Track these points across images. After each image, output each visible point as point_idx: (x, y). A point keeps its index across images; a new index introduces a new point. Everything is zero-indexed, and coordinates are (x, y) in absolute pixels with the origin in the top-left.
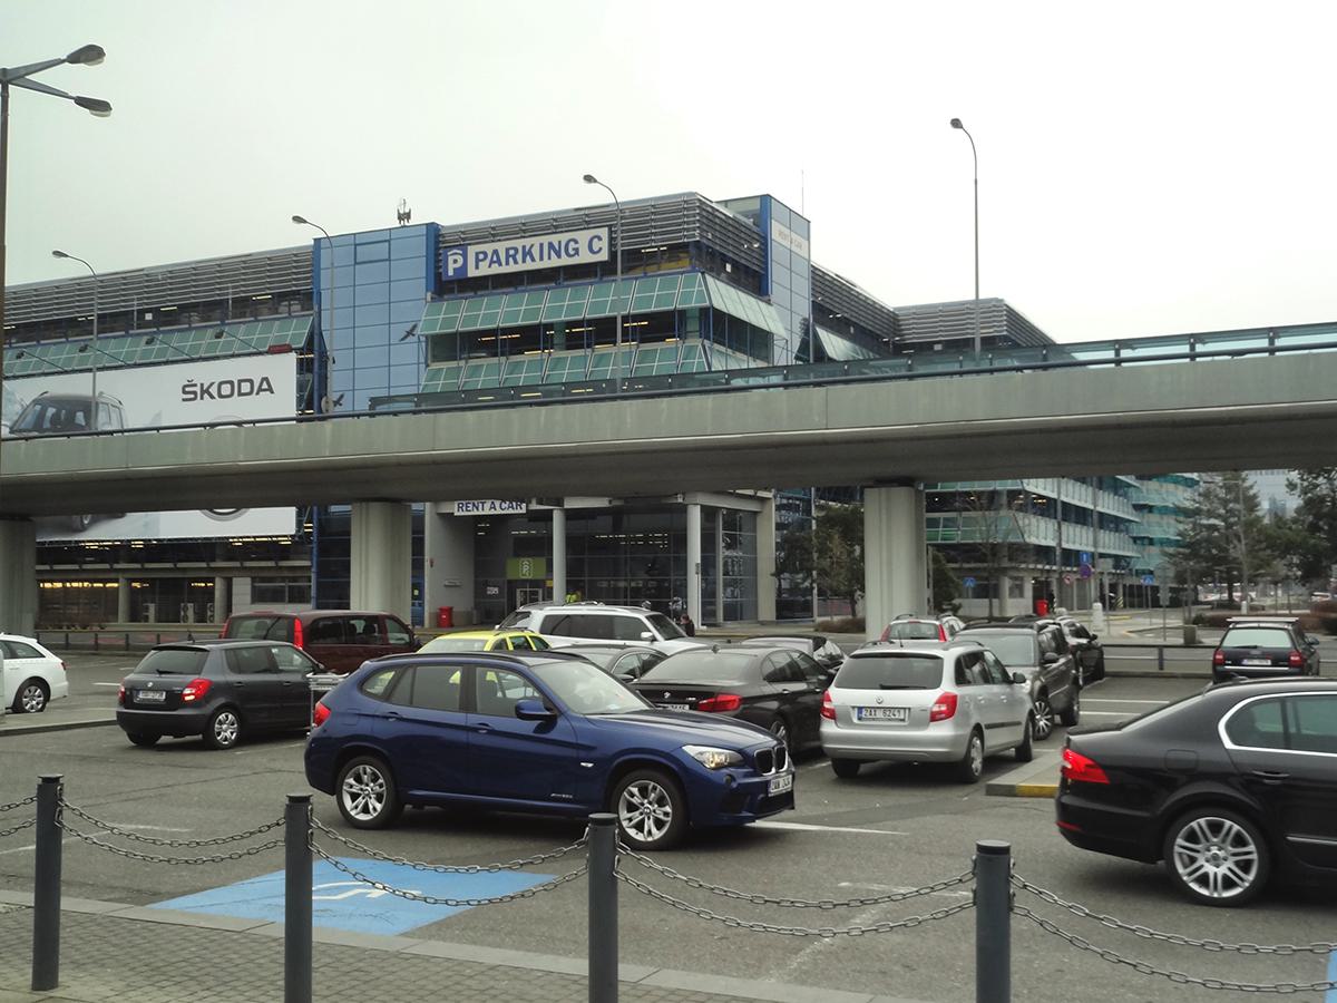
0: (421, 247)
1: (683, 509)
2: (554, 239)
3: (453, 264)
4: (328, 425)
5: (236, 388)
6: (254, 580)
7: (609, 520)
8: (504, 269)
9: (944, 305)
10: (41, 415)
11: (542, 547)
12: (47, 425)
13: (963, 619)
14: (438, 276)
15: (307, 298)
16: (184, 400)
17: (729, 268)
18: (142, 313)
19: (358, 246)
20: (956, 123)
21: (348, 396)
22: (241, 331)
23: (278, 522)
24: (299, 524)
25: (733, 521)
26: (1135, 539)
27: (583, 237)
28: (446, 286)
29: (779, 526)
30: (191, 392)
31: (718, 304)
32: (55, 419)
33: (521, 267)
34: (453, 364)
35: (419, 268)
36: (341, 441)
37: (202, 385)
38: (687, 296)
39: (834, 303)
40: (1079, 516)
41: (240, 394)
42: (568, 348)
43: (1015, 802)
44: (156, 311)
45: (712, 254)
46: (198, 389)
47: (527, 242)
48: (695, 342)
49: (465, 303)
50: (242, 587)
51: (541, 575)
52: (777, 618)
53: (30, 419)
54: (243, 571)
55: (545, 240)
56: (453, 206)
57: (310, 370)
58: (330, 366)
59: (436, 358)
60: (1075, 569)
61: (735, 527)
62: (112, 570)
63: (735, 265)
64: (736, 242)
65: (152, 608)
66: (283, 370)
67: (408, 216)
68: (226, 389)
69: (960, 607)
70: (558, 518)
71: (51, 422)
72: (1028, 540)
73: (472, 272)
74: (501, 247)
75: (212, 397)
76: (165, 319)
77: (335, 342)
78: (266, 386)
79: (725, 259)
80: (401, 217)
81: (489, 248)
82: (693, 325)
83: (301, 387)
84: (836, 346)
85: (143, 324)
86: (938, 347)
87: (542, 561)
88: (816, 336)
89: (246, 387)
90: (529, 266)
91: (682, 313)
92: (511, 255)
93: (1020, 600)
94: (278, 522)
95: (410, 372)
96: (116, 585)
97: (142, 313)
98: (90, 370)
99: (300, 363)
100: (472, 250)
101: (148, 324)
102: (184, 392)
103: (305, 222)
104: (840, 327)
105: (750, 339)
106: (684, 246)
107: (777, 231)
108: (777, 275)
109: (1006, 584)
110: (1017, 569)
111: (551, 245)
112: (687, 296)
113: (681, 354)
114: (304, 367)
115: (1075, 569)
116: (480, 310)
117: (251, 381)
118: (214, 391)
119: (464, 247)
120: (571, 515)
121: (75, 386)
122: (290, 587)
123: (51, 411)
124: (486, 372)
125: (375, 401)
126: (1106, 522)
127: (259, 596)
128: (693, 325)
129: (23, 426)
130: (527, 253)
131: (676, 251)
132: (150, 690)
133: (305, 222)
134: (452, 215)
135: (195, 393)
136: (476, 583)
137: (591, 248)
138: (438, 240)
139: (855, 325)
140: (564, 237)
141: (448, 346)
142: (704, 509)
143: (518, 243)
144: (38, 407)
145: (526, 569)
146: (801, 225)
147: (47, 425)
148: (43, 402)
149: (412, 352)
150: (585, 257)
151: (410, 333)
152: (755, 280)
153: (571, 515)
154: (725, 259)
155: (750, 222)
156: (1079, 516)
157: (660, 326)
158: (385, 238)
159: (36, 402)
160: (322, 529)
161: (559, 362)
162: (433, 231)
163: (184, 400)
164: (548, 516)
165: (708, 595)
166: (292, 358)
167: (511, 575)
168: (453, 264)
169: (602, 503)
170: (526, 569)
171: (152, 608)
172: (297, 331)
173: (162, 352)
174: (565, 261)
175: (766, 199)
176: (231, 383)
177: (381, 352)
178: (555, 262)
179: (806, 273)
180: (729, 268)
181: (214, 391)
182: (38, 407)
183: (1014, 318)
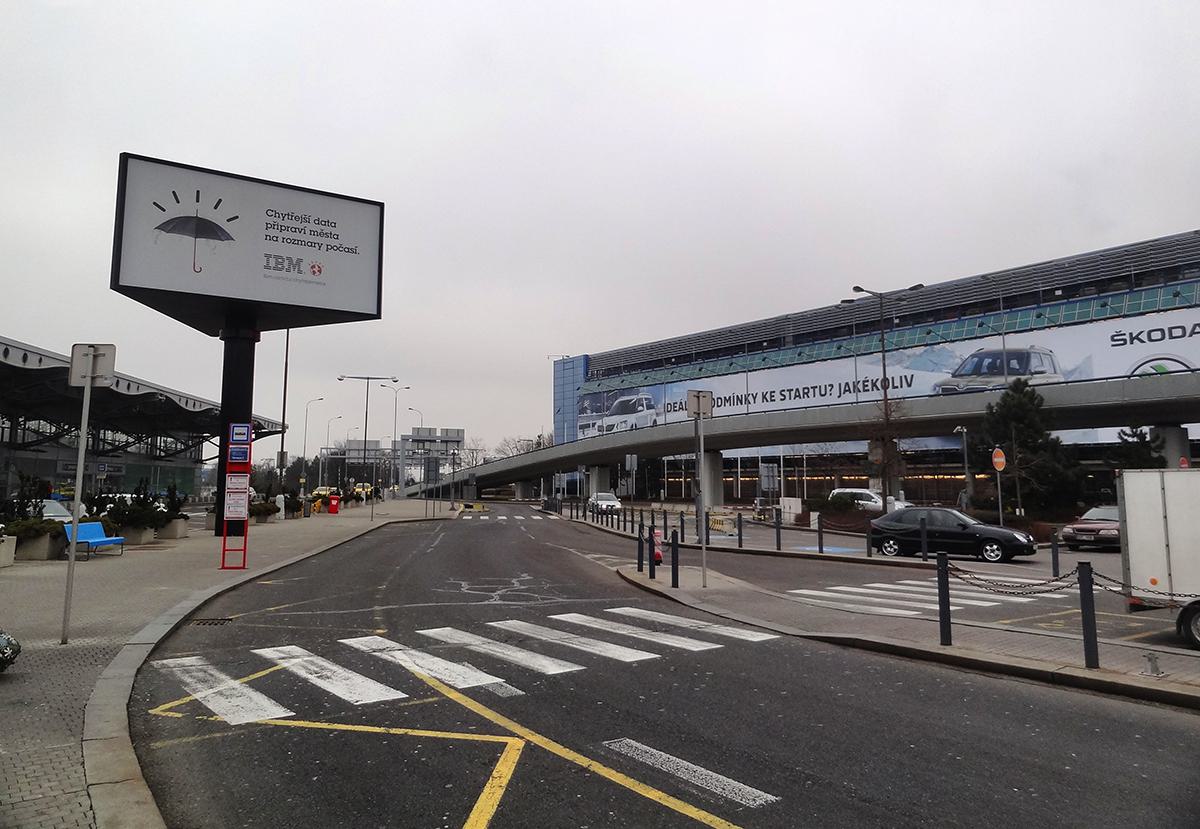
5: (1167, 334)
12: (985, 370)
16: (1113, 345)
30: (1118, 340)
37: (1131, 334)
41: (1171, 337)
43: (912, 573)
46: (1127, 337)
52: (1116, 505)
53: (969, 367)
71: (988, 368)
75: (1143, 342)
96: (964, 477)
98: (1000, 334)
102: (1113, 340)
103: (863, 290)
116: (1141, 299)
117: (1183, 328)
118: (1144, 337)
121: (1016, 342)
122: (784, 466)
123: (987, 361)
129: (962, 373)
132: (937, 537)
133: (863, 290)
135: (1125, 340)
144: (976, 359)
147: (985, 370)
148: (980, 356)
159: (973, 356)
163: (1113, 345)
176: (1162, 330)
181: (1144, 337)
182: (976, 359)
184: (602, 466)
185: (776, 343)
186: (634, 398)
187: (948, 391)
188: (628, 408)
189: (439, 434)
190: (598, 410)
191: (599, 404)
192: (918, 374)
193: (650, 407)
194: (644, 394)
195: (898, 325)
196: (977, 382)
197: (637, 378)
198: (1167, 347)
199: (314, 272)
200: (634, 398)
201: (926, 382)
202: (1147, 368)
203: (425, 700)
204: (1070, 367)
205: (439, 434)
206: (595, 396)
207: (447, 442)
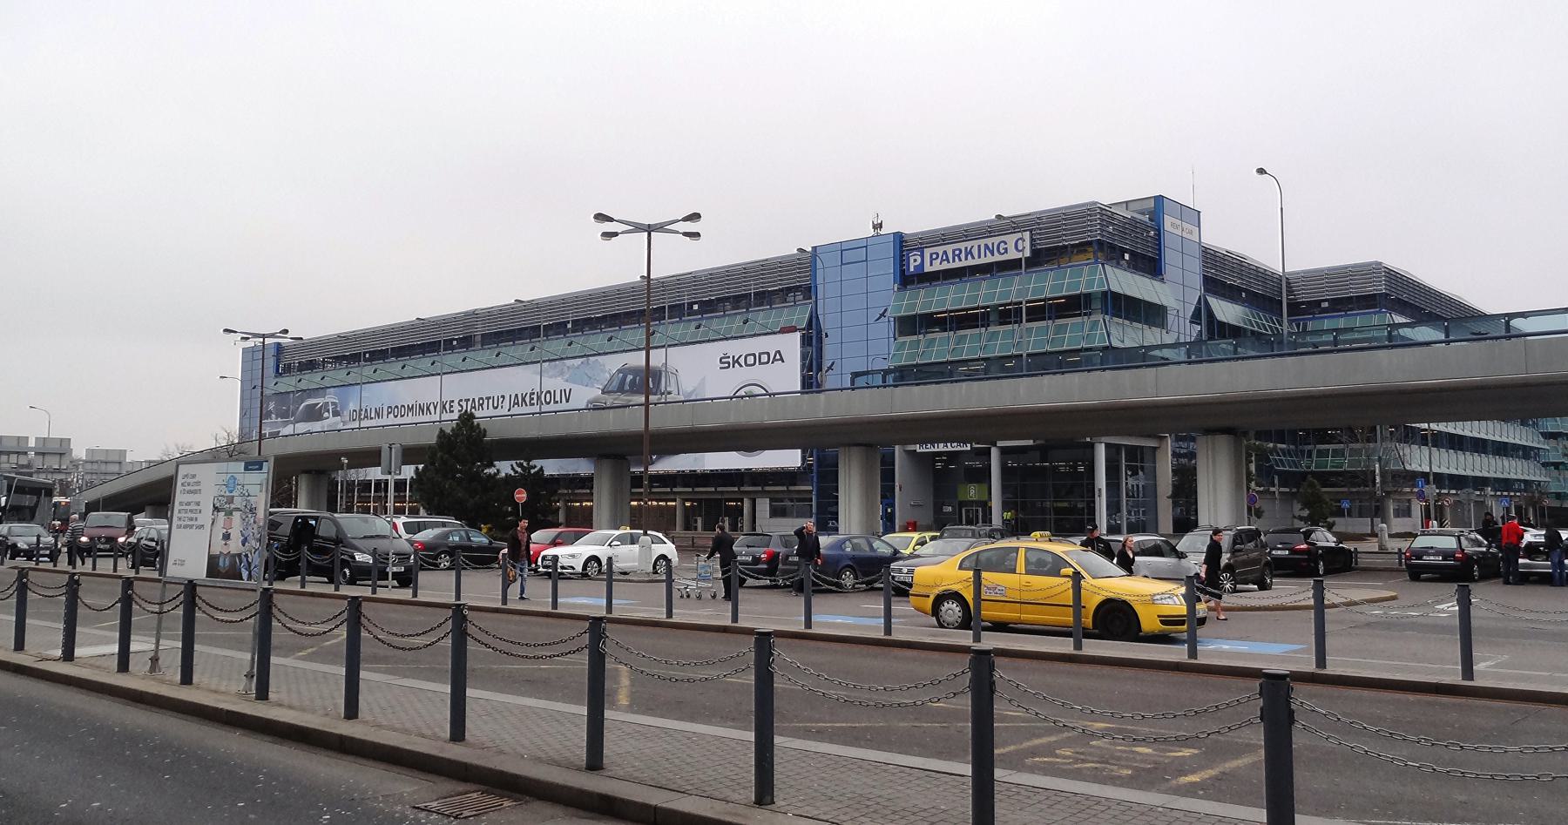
0: (890, 250)
1: (1092, 446)
2: (989, 241)
3: (913, 262)
4: (822, 396)
5: (757, 359)
6: (772, 500)
7: (1038, 454)
8: (952, 265)
9: (1329, 269)
10: (624, 379)
11: (983, 476)
12: (627, 387)
13: (1335, 534)
14: (902, 272)
15: (808, 291)
17: (1127, 256)
18: (691, 305)
19: (844, 251)
20: (1261, 171)
21: (838, 362)
22: (761, 316)
23: (790, 459)
24: (804, 459)
25: (1133, 453)
26: (1545, 465)
27: (1011, 239)
28: (907, 279)
29: (1175, 455)
30: (727, 363)
31: (1115, 288)
32: (633, 382)
33: (964, 264)
34: (914, 338)
35: (889, 267)
36: (838, 404)
38: (1090, 283)
39: (1224, 276)
40: (1502, 449)
42: (1001, 324)
44: (701, 303)
45: (1112, 247)
47: (969, 244)
48: (1099, 317)
49: (922, 292)
50: (764, 506)
51: (985, 498)
53: (615, 383)
54: (764, 494)
55: (982, 242)
56: (915, 217)
57: (810, 345)
58: (826, 341)
59: (902, 334)
60: (505, 468)
61: (1139, 459)
62: (672, 493)
63: (1132, 254)
64: (1136, 236)
65: (700, 520)
66: (791, 345)
67: (880, 226)
68: (751, 360)
69: (1333, 524)
70: (994, 453)
72: (1408, 467)
73: (928, 268)
74: (949, 249)
76: (708, 307)
77: (828, 323)
78: (779, 357)
79: (1124, 251)
80: (875, 227)
81: (940, 250)
82: (1097, 305)
83: (804, 357)
84: (1227, 311)
85: (691, 313)
86: (1325, 305)
87: (985, 487)
88: (1206, 302)
89: (764, 358)
90: (970, 262)
91: (1088, 296)
92: (957, 255)
93: (1406, 519)
94: (790, 459)
95: (886, 350)
97: (691, 305)
99: (803, 337)
100: (927, 252)
101: (696, 313)
104: (1230, 293)
105: (1152, 314)
106: (1089, 243)
107: (1168, 223)
108: (1170, 258)
109: (1391, 507)
110: (1401, 493)
111: (986, 246)
112: (1090, 283)
113: (1086, 329)
114: (806, 341)
115: (505, 468)
118: (742, 361)
119: (921, 250)
120: (1004, 452)
123: (630, 377)
124: (939, 347)
125: (856, 375)
126: (1525, 452)
127: (776, 512)
128: (1097, 305)
130: (969, 253)
131: (1082, 247)
134: (913, 223)
136: (935, 504)
137: (1017, 247)
138: (902, 245)
139: (1246, 290)
140: (996, 240)
141: (910, 325)
142: (1108, 446)
143: (962, 246)
145: (972, 492)
146: (1195, 216)
147: (627, 387)
148: (624, 371)
149: (885, 329)
150: (1013, 255)
151: (883, 315)
152: (1151, 265)
153: (1004, 452)
154: (1124, 251)
155: (1146, 218)
156: (1502, 449)
157: (1074, 305)
158: (863, 245)
159: (619, 371)
160: (820, 461)
161: (994, 335)
162: (899, 238)
164: (987, 453)
165: (1114, 508)
166: (798, 334)
167: (961, 498)
168: (913, 262)
169: (1031, 442)
170: (972, 492)
171: (700, 520)
172: (800, 316)
173: (706, 334)
174: (998, 258)
175: (1159, 199)
177: (864, 334)
178: (989, 259)
179: (1197, 253)
180: (1127, 256)
181: (742, 361)
183: (1393, 277)
184: (868, 446)
185: (467, 342)
186: (320, 401)
187: (595, 407)
188: (314, 414)
189: (32, 443)
190: (284, 415)
191: (286, 406)
192: (575, 387)
193: (336, 414)
194: (331, 398)
195: (1325, 310)
196: (623, 399)
197: (338, 374)
198: (759, 374)
199: (695, 235)
200: (320, 401)
201: (584, 395)
202: (742, 393)
203: (1212, 772)
204: (690, 389)
205: (32, 443)
206: (281, 396)
207: (44, 454)
